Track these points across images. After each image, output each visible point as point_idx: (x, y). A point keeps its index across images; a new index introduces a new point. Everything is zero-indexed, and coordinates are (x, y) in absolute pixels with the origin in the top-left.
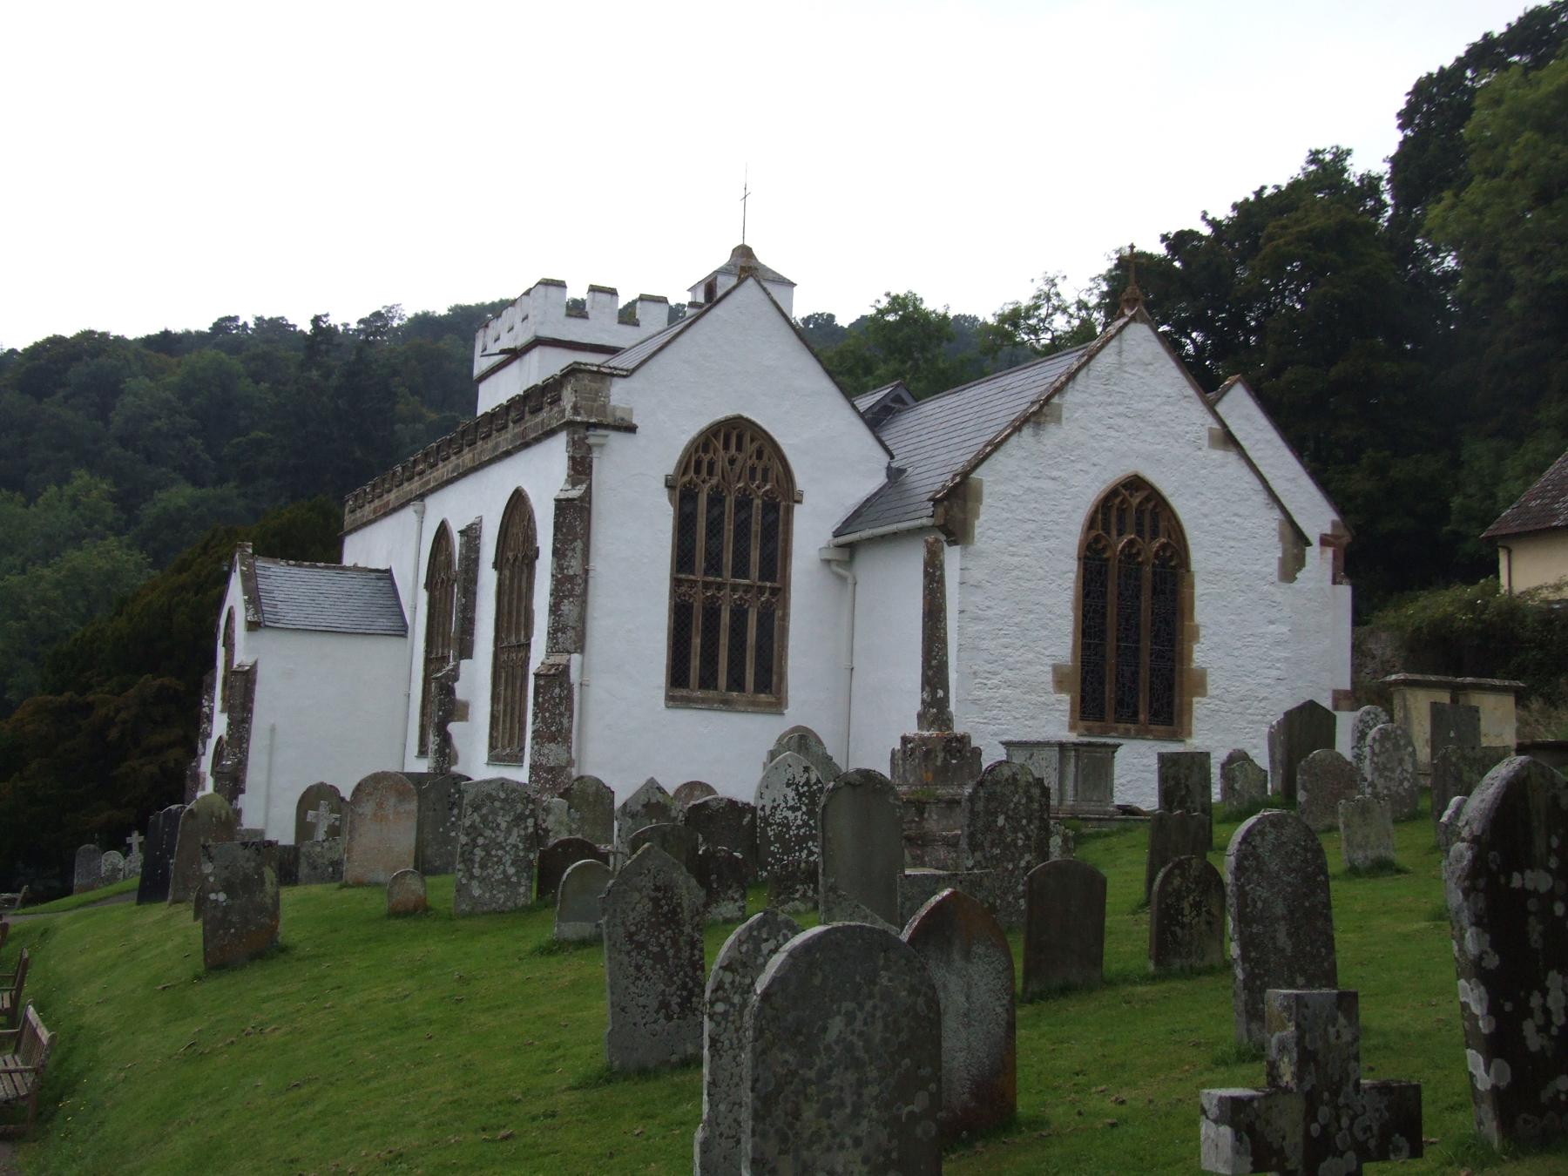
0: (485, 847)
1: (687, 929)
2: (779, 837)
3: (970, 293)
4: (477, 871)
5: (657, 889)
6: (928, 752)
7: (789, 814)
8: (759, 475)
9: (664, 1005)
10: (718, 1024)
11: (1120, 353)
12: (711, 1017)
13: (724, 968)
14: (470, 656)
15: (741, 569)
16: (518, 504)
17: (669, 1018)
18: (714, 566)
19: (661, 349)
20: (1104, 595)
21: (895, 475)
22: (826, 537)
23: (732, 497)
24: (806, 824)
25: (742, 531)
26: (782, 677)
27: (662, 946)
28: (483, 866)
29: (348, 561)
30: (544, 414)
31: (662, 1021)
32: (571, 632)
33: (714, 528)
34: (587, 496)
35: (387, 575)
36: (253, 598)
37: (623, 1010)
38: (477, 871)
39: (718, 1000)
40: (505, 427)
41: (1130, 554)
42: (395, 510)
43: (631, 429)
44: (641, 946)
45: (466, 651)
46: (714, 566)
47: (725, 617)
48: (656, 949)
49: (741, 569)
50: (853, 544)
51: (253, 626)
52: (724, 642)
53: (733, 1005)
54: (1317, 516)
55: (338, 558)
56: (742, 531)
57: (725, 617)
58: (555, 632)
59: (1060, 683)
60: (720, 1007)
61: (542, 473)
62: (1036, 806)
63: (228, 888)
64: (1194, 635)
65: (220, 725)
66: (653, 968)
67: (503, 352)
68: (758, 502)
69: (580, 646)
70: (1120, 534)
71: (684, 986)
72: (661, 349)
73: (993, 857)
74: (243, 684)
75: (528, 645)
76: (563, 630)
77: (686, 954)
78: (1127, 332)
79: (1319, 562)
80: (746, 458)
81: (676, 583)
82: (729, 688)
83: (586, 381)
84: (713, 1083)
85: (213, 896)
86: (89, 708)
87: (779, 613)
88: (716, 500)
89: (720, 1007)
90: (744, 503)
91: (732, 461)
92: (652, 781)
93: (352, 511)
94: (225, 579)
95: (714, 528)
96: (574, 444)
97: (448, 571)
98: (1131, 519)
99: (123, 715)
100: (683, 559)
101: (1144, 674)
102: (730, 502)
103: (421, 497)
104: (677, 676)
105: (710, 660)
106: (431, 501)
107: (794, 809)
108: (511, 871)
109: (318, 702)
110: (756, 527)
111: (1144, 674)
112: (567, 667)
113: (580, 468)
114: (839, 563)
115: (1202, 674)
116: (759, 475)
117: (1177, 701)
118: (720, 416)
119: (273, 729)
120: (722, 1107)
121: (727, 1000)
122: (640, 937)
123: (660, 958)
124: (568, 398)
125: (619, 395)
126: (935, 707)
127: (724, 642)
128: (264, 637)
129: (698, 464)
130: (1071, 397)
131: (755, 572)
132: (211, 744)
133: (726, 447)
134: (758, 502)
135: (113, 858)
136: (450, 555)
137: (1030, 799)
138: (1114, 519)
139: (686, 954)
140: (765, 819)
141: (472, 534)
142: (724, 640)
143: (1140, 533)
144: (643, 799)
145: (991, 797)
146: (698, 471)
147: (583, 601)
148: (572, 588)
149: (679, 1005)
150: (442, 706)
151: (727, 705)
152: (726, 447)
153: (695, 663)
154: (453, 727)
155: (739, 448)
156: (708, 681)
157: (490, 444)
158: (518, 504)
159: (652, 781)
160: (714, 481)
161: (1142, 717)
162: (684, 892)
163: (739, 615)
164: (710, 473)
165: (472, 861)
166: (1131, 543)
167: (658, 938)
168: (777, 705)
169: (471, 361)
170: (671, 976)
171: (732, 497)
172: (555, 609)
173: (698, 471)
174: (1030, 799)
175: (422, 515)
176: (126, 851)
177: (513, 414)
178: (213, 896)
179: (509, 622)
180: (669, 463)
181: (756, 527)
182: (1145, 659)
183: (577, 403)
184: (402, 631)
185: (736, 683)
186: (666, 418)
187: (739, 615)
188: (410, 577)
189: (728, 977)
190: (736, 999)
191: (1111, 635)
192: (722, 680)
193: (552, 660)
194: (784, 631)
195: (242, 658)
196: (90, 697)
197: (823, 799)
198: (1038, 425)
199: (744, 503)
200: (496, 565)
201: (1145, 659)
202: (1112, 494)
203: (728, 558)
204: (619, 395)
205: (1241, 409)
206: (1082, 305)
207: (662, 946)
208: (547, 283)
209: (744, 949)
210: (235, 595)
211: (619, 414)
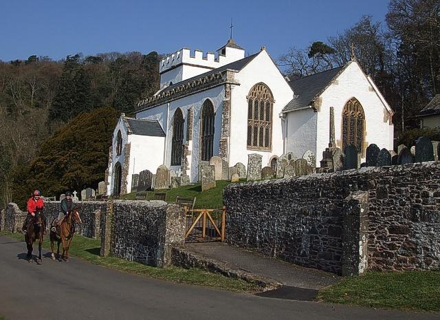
15: (262, 119)
16: (208, 104)
18: (256, 118)
19: (193, 65)
25: (262, 109)
43: (239, 85)
46: (256, 118)
47: (259, 129)
49: (262, 119)
56: (262, 109)
57: (259, 129)
63: (206, 175)
72: (193, 65)
81: (249, 121)
88: (256, 102)
93: (354, 117)
100: (250, 116)
104: (249, 143)
105: (255, 140)
130: (375, 93)
131: (265, 119)
158: (208, 104)
163: (262, 129)
185: (261, 145)
187: (262, 129)
199: (262, 103)
203: (259, 116)
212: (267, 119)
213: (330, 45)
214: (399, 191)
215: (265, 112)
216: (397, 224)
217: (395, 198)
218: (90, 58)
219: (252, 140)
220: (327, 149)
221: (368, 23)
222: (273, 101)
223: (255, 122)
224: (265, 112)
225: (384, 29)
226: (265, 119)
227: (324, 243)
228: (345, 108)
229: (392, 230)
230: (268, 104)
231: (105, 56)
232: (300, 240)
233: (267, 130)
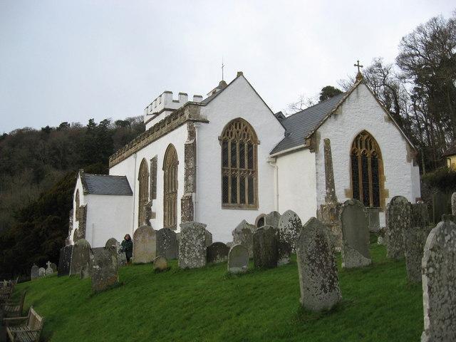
0: (189, 246)
1: (330, 253)
2: (287, 239)
4: (186, 255)
5: (318, 236)
6: (331, 209)
7: (290, 231)
8: (246, 137)
9: (323, 286)
10: (431, 279)
11: (357, 93)
12: (428, 275)
13: (431, 250)
14: (155, 198)
15: (242, 165)
16: (171, 149)
17: (326, 292)
18: (234, 164)
20: (357, 167)
21: (287, 135)
22: (268, 155)
23: (239, 145)
24: (296, 234)
25: (242, 153)
26: (257, 199)
27: (321, 261)
28: (188, 253)
30: (178, 119)
31: (323, 293)
32: (192, 185)
33: (234, 153)
34: (194, 144)
35: (125, 178)
36: (84, 183)
37: (308, 289)
38: (186, 255)
39: (430, 266)
40: (164, 126)
41: (364, 155)
42: (126, 158)
43: (208, 122)
44: (313, 261)
45: (154, 196)
46: (234, 164)
48: (319, 262)
49: (242, 165)
50: (280, 151)
51: (85, 194)
52: (238, 187)
53: (436, 269)
55: (107, 172)
56: (242, 153)
58: (186, 186)
60: (431, 270)
61: (179, 138)
62: (409, 212)
63: (100, 264)
64: (384, 179)
65: (76, 225)
66: (318, 270)
67: (154, 114)
68: (246, 144)
69: (194, 190)
70: (361, 148)
71: (330, 278)
73: (397, 231)
74: (83, 212)
75: (176, 192)
76: (189, 185)
77: (330, 264)
78: (359, 87)
81: (223, 170)
82: (241, 203)
83: (192, 107)
84: (431, 310)
85: (94, 267)
86: (32, 226)
87: (254, 179)
88: (233, 144)
89: (431, 270)
90: (242, 145)
91: (238, 132)
92: (244, 221)
94: (76, 180)
95: (234, 153)
97: (146, 174)
98: (364, 144)
99: (44, 227)
100: (224, 163)
102: (238, 144)
103: (135, 152)
104: (225, 200)
106: (138, 153)
107: (291, 229)
108: (198, 254)
109: (105, 219)
110: (246, 152)
112: (191, 197)
113: (192, 134)
114: (273, 163)
115: (388, 191)
116: (246, 137)
117: (380, 200)
118: (234, 118)
120: (435, 322)
121: (433, 266)
122: (313, 257)
123: (321, 266)
124: (187, 114)
125: (203, 111)
127: (238, 187)
128: (90, 196)
129: (228, 133)
131: (246, 166)
132: (73, 232)
133: (236, 128)
134: (246, 144)
135: (42, 270)
136: (146, 169)
137: (407, 210)
138: (359, 144)
139: (330, 264)
140: (282, 233)
141: (154, 161)
142: (238, 188)
143: (367, 148)
144: (242, 227)
145: (395, 209)
146: (228, 135)
147: (194, 176)
148: (191, 172)
149: (329, 286)
150: (146, 213)
151: (240, 208)
152: (236, 128)
154: (151, 220)
155: (240, 128)
156: (234, 201)
157: (159, 132)
158: (171, 149)
159: (244, 221)
160: (233, 138)
161: (371, 205)
162: (328, 237)
164: (231, 136)
165: (185, 252)
166: (364, 151)
167: (319, 257)
168: (256, 207)
170: (325, 274)
171: (239, 145)
172: (186, 179)
173: (228, 135)
174: (407, 210)
175: (136, 158)
176: (46, 267)
177: (167, 122)
178: (94, 267)
179: (168, 186)
180: (219, 132)
183: (186, 114)
184: (131, 193)
185: (243, 201)
186: (218, 118)
187: (242, 180)
188: (133, 180)
189: (433, 254)
190: (437, 266)
193: (188, 194)
194: (257, 184)
195: (82, 203)
196: (33, 223)
197: (341, 211)
198: (336, 115)
199: (242, 145)
200: (163, 169)
202: (358, 136)
203: (238, 162)
204: (203, 111)
207: (321, 261)
208: (166, 92)
209: (438, 239)
210: (79, 185)
211: (203, 117)
213: (341, 89)
218: (118, 122)
219: (230, 195)
220: (276, 214)
221: (379, 65)
222: (257, 143)
223: (232, 171)
225: (396, 71)
226: (246, 166)
228: (353, 146)
230: (250, 146)
231: (133, 120)
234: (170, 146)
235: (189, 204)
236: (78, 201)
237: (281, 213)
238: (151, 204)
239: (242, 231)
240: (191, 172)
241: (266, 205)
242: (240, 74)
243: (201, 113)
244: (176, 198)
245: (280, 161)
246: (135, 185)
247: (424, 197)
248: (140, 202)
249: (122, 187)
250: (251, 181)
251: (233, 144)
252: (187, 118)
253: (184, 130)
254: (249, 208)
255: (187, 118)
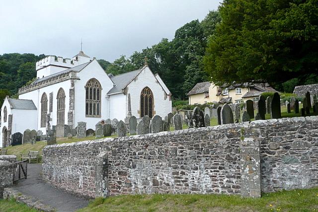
3: (84, 53)
15: (94, 99)
18: (91, 98)
21: (114, 86)
29: (19, 98)
32: (72, 107)
41: (146, 97)
45: (51, 110)
46: (91, 98)
47: (93, 105)
49: (94, 99)
50: (110, 95)
52: (92, 109)
54: (168, 92)
57: (93, 105)
59: (138, 113)
61: (66, 86)
63: (50, 136)
79: (168, 97)
80: (95, 84)
88: (91, 89)
93: (21, 91)
96: (72, 81)
100: (87, 97)
101: (148, 111)
104: (87, 113)
111: (148, 111)
113: (73, 85)
119: (16, 124)
124: (70, 75)
125: (78, 75)
126: (130, 113)
127: (92, 109)
130: (139, 76)
131: (96, 99)
136: (46, 98)
141: (51, 94)
148: (72, 101)
153: (89, 111)
157: (54, 81)
168: (100, 117)
169: (35, 67)
181: (96, 93)
182: (148, 109)
185: (94, 114)
187: (95, 105)
191: (144, 107)
192: (93, 113)
196: (244, 29)
199: (95, 90)
201: (148, 109)
203: (93, 97)
204: (78, 75)
205: (158, 77)
206: (128, 61)
212: (98, 99)
214: (123, 152)
215: (96, 95)
216: (121, 170)
217: (121, 155)
224: (96, 95)
227: (90, 181)
229: (119, 173)
230: (98, 90)
232: (78, 179)
233: (98, 105)
234: (44, 94)
235: (71, 115)
236: (5, 111)
237: (112, 119)
238: (50, 114)
239: (98, 126)
240: (72, 101)
241: (104, 116)
242: (94, 58)
243: (77, 76)
244: (64, 113)
245: (111, 98)
246: (39, 105)
247: (207, 21)
248: (42, 113)
249: (31, 105)
250: (98, 105)
251: (91, 89)
252: (71, 77)
253: (69, 82)
254: (97, 117)
255: (71, 77)
